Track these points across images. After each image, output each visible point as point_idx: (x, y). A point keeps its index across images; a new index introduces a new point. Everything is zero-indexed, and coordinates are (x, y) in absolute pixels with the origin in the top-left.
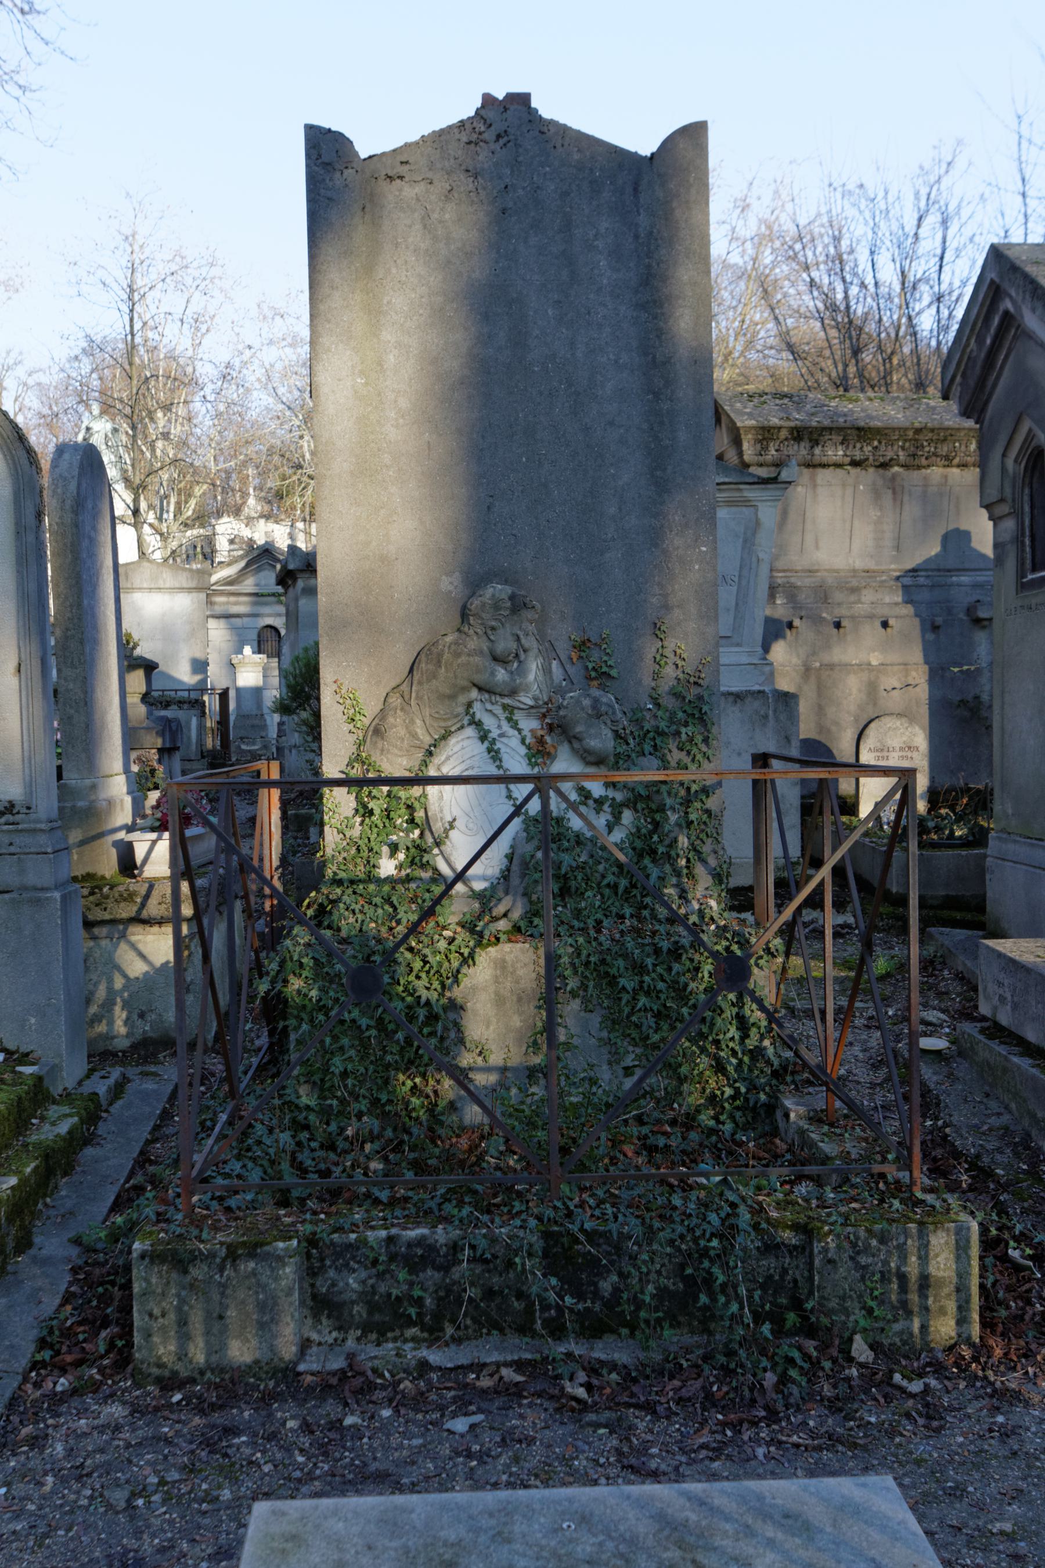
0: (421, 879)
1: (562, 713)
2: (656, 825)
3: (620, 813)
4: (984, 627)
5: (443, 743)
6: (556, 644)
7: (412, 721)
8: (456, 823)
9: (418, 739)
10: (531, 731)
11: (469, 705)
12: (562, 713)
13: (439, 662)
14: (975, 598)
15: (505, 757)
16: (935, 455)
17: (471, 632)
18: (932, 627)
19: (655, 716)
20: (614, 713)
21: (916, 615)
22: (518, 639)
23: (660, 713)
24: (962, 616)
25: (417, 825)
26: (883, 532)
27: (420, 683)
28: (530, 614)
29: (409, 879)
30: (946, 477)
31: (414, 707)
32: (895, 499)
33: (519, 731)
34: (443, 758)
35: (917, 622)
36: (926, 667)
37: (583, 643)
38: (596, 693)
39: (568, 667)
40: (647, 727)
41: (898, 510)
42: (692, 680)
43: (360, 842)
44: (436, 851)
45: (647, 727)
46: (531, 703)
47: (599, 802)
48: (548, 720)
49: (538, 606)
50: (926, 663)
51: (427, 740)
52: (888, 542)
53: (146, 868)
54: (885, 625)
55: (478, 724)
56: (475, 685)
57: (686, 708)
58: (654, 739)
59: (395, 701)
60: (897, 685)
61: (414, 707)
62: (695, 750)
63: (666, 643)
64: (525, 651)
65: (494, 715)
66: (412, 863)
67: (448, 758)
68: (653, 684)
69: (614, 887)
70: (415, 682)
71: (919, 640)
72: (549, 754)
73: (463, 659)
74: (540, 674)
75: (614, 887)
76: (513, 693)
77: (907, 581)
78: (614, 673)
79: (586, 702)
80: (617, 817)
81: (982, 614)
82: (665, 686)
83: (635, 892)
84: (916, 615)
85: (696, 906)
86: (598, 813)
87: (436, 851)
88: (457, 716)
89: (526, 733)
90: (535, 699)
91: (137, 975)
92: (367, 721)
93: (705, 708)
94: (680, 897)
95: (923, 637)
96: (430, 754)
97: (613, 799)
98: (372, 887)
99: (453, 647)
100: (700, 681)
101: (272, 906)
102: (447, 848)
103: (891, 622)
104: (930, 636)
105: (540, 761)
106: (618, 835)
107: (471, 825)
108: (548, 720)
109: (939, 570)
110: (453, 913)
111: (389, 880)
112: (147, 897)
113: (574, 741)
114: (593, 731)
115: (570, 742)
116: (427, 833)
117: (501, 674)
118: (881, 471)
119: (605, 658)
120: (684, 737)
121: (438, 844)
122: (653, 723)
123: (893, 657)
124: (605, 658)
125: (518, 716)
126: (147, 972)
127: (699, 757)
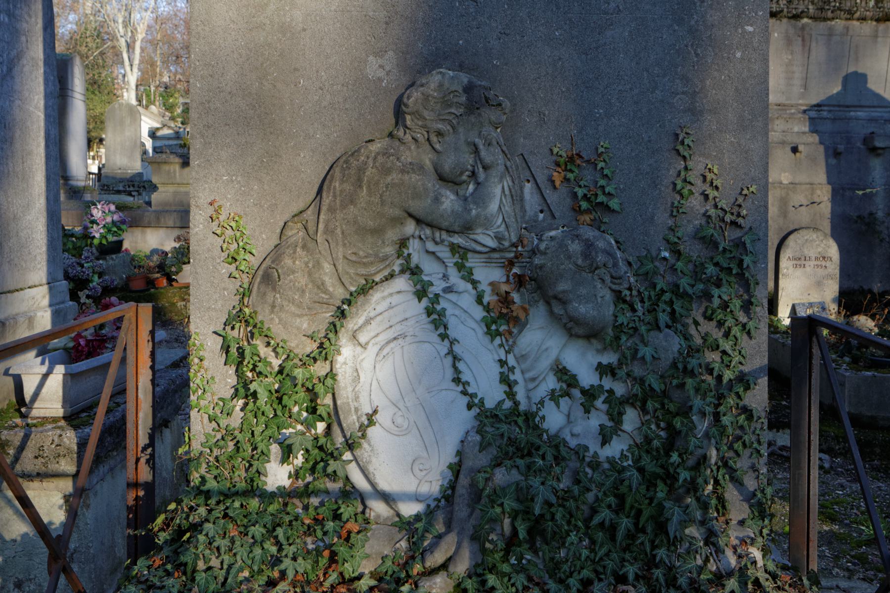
0: (327, 492)
1: (537, 261)
2: (673, 434)
3: (621, 414)
4: (878, 155)
5: (361, 298)
6: (531, 159)
7: (318, 265)
8: (378, 417)
9: (326, 292)
10: (492, 284)
11: (403, 243)
12: (537, 261)
13: (360, 179)
14: (869, 131)
15: (452, 322)
16: (840, 9)
17: (408, 137)
18: (834, 154)
19: (673, 269)
20: (615, 265)
21: (821, 143)
22: (476, 151)
23: (680, 265)
24: (859, 144)
25: (322, 419)
26: (793, 72)
27: (332, 210)
28: (492, 115)
29: (306, 492)
30: (847, 28)
31: (323, 246)
32: (804, 46)
33: (475, 283)
34: (361, 321)
35: (821, 149)
36: (829, 187)
37: (571, 159)
38: (590, 233)
39: (548, 192)
40: (661, 284)
41: (806, 55)
42: (728, 218)
43: (240, 437)
44: (347, 456)
45: (661, 284)
46: (492, 243)
47: (590, 394)
48: (515, 270)
49: (507, 104)
50: (829, 183)
51: (340, 293)
52: (797, 82)
53: (36, 405)
54: (795, 150)
55: (414, 272)
56: (411, 215)
57: (719, 259)
58: (671, 303)
59: (296, 233)
60: (805, 202)
61: (323, 246)
62: (730, 322)
63: (690, 164)
64: (485, 168)
65: (438, 258)
66: (313, 470)
67: (368, 322)
68: (670, 222)
69: (611, 530)
70: (324, 209)
71: (823, 164)
72: (516, 320)
73: (394, 177)
74: (507, 202)
75: (611, 530)
76: (467, 229)
77: (813, 114)
78: (614, 204)
79: (575, 247)
80: (616, 418)
81: (879, 143)
82: (688, 228)
83: (641, 538)
84: (821, 143)
85: (733, 561)
86: (587, 411)
87: (347, 456)
88: (385, 258)
89: (484, 286)
90: (499, 238)
91: (14, 537)
92: (255, 262)
93: (747, 260)
94: (706, 543)
95: (827, 161)
96: (342, 314)
97: (611, 392)
98: (254, 504)
99: (380, 159)
100: (740, 221)
101: (137, 498)
102: (364, 451)
103: (801, 148)
104: (833, 161)
105: (503, 328)
106: (616, 448)
107: (399, 420)
108: (515, 270)
109: (839, 106)
110: (367, 557)
111: (282, 492)
112: (21, 448)
113: (554, 303)
114: (583, 291)
115: (548, 303)
116: (336, 429)
117: (449, 201)
118: (793, 21)
119: (602, 182)
120: (716, 302)
121: (351, 446)
122: (669, 278)
123: (802, 178)
124: (602, 182)
125: (472, 261)
126: (27, 534)
127: (736, 331)
